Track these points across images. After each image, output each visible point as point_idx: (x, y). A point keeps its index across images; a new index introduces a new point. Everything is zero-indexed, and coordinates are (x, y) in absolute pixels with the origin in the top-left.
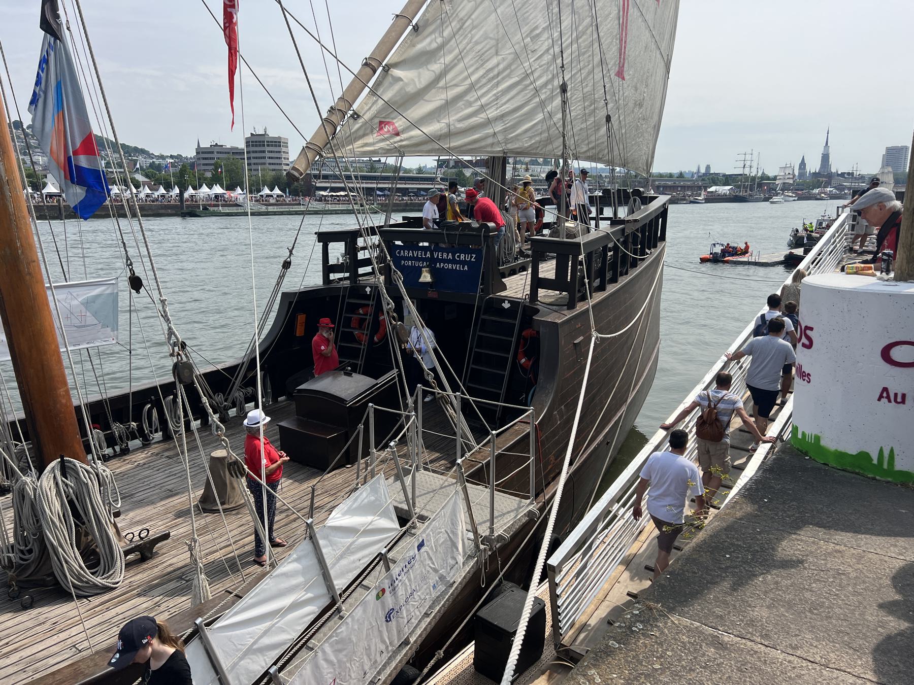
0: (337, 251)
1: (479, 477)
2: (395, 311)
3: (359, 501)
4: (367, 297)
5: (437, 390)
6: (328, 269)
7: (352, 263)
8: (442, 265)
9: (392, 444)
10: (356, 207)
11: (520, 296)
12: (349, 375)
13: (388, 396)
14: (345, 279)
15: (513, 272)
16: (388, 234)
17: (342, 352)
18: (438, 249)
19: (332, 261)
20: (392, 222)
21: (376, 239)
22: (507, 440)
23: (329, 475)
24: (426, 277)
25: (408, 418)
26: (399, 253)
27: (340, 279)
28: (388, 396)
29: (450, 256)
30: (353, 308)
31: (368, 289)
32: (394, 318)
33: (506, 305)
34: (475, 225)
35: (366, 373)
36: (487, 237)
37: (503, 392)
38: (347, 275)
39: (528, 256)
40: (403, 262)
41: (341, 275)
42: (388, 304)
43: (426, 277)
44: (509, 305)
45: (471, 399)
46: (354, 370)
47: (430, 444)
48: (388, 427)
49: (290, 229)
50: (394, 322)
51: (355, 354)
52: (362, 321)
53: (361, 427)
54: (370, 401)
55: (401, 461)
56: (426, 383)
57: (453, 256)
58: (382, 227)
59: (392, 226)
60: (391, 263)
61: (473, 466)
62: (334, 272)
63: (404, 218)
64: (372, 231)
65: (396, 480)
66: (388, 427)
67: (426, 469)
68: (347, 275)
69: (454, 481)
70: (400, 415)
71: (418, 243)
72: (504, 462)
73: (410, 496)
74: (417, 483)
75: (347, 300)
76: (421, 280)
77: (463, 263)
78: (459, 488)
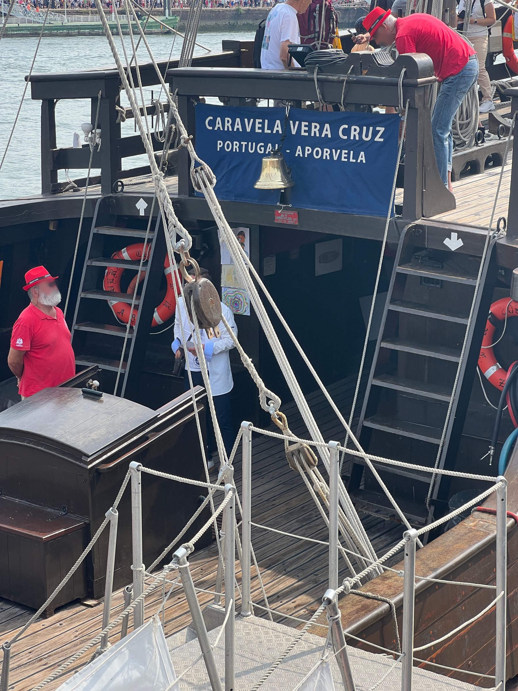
0: (74, 118)
1: (378, 634)
2: (194, 253)
3: (105, 678)
4: (140, 223)
5: (288, 436)
6: (55, 159)
7: (111, 146)
8: (308, 150)
9: (181, 552)
10: (122, 20)
11: (484, 222)
12: (94, 396)
13: (177, 450)
14: (93, 181)
15: (471, 168)
16: (186, 82)
17: (82, 344)
18: (299, 113)
19: (64, 141)
20: (198, 53)
21: (161, 93)
22: (448, 552)
23: (47, 622)
24: (271, 177)
25: (220, 496)
26: (212, 123)
27: (81, 183)
28: (177, 450)
29: (327, 131)
30: (109, 247)
31: (141, 206)
32: (190, 268)
33: (454, 243)
34: (384, 58)
35: (135, 394)
36: (410, 88)
37: (443, 441)
38: (96, 172)
39: (505, 131)
40: (220, 144)
41: (82, 173)
42: (179, 239)
43: (271, 177)
44: (459, 243)
45: (368, 458)
46: (107, 387)
47: (270, 557)
48: (174, 514)
49: (9, 66)
50: (190, 279)
51: (109, 349)
52: (127, 277)
53: (113, 515)
54: (134, 458)
55: (203, 597)
56: (264, 420)
57: (334, 130)
58: (175, 64)
59: (197, 62)
60: (190, 147)
61: (366, 609)
62: (66, 166)
63: (226, 45)
64: (148, 75)
65: (190, 637)
66: (174, 514)
67: (259, 613)
68: (96, 172)
69: (323, 641)
70: (205, 491)
71: (255, 100)
72: (434, 603)
73: (221, 673)
74: (236, 643)
75: (94, 230)
76: (259, 185)
77: (356, 146)
78: (330, 656)
